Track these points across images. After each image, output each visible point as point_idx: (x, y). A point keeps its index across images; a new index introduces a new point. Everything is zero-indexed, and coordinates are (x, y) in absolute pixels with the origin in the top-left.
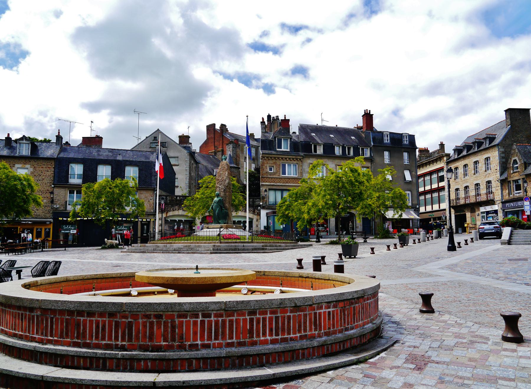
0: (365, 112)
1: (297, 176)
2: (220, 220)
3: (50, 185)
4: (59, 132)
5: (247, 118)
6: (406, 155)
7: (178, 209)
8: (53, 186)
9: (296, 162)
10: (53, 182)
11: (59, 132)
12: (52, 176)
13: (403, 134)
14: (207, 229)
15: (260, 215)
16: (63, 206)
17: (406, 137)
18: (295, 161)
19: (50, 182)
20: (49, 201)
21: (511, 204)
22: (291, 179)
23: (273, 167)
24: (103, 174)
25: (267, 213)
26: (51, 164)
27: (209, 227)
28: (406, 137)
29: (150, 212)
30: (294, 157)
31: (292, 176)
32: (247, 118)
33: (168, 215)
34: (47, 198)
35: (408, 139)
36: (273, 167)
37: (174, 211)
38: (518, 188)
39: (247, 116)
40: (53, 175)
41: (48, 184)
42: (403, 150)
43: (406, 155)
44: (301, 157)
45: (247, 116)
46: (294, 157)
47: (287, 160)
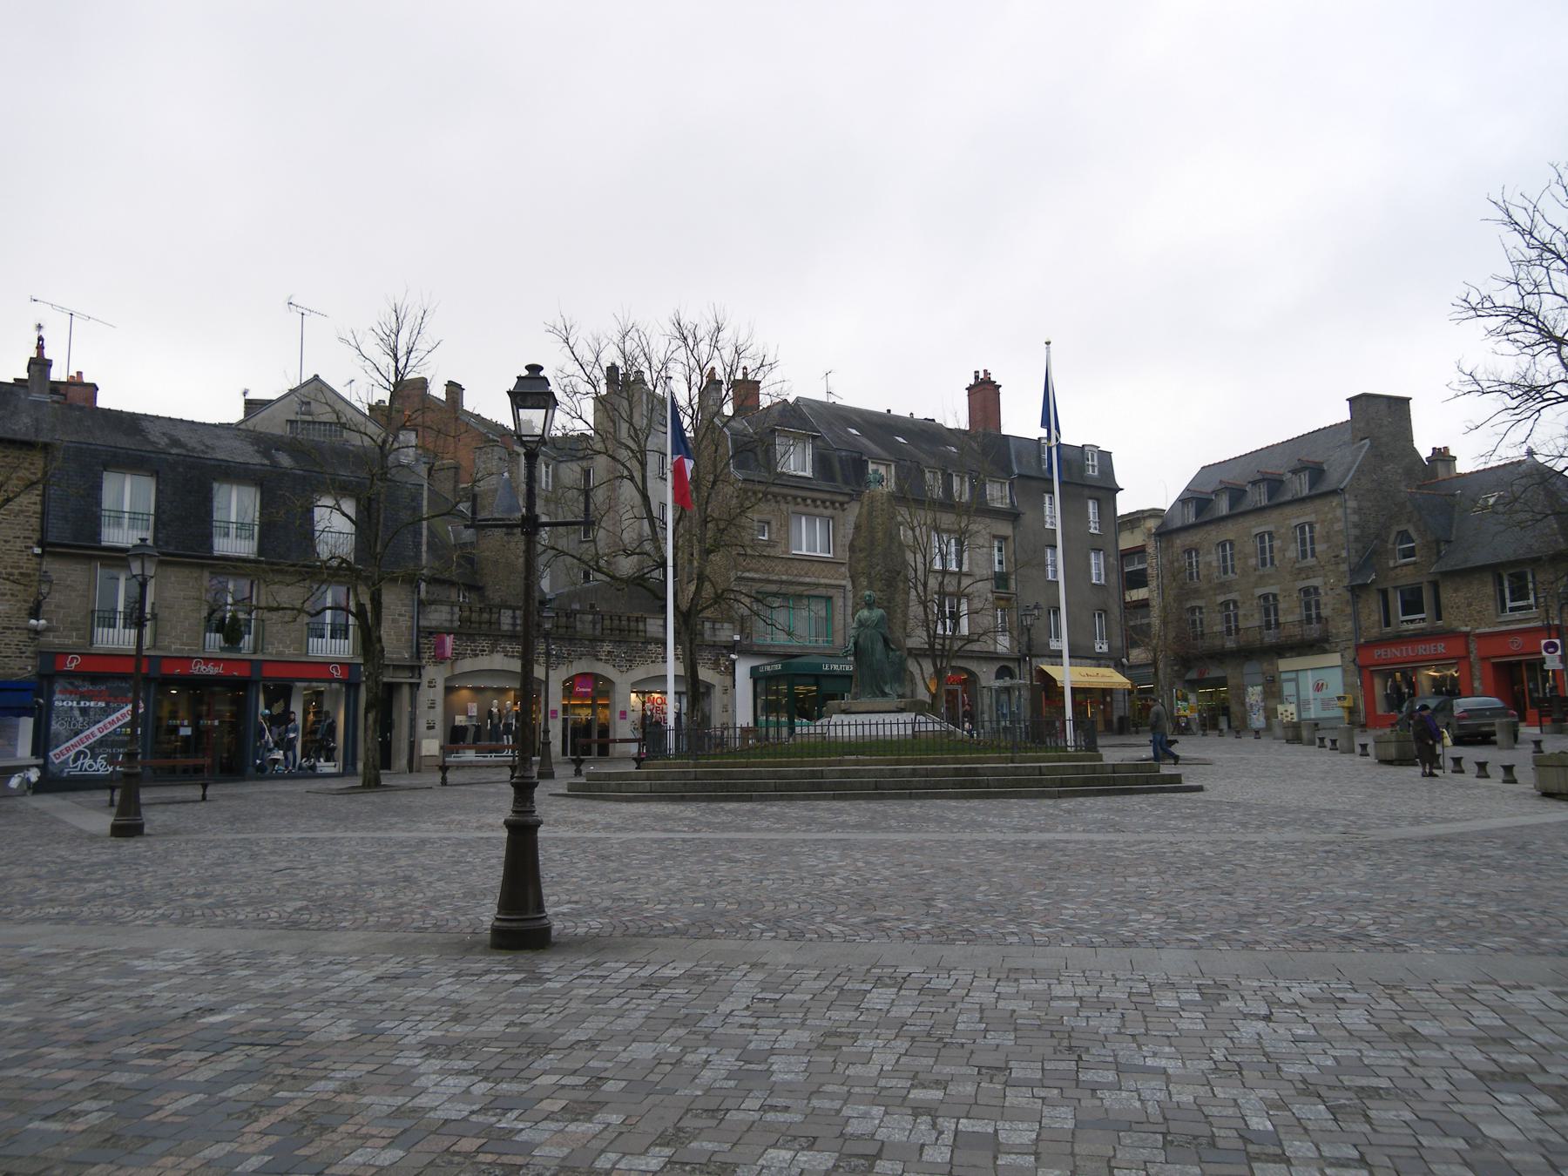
0: (977, 377)
1: (831, 555)
2: (886, 683)
3: (27, 547)
4: (40, 347)
5: (1048, 352)
6: (1092, 507)
7: (492, 652)
8: (38, 550)
9: (828, 512)
10: (36, 536)
11: (40, 347)
12: (35, 513)
13: (1086, 448)
14: (843, 716)
15: (733, 673)
16: (78, 630)
17: (1092, 455)
18: (826, 508)
19: (27, 534)
20: (19, 610)
21: (1394, 650)
22: (816, 564)
23: (768, 523)
24: (229, 516)
25: (753, 669)
26: (32, 464)
27: (853, 709)
28: (1092, 455)
29: (397, 659)
30: (827, 496)
31: (804, 552)
32: (1048, 352)
33: (457, 671)
34: (12, 595)
35: (1096, 463)
36: (768, 523)
37: (476, 655)
38: (1412, 604)
39: (1048, 343)
40: (38, 508)
41: (19, 544)
42: (1086, 492)
43: (1092, 507)
44: (846, 499)
45: (1048, 343)
46: (827, 496)
47: (807, 505)
